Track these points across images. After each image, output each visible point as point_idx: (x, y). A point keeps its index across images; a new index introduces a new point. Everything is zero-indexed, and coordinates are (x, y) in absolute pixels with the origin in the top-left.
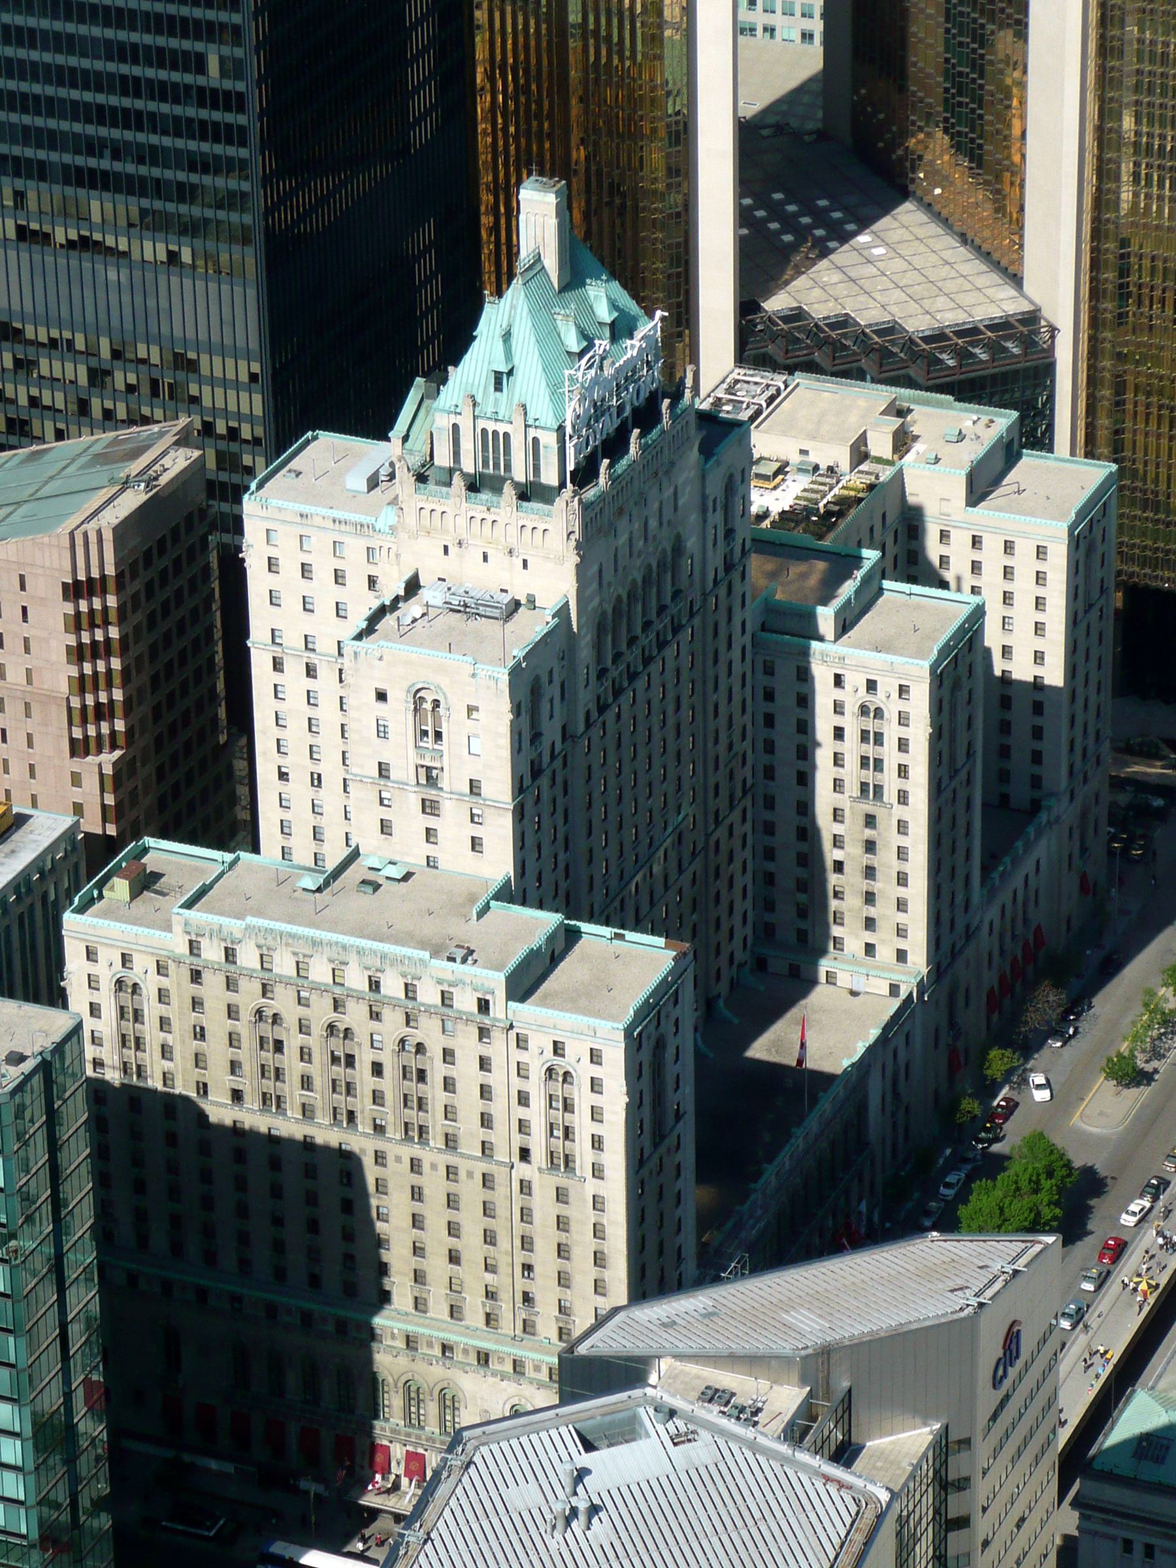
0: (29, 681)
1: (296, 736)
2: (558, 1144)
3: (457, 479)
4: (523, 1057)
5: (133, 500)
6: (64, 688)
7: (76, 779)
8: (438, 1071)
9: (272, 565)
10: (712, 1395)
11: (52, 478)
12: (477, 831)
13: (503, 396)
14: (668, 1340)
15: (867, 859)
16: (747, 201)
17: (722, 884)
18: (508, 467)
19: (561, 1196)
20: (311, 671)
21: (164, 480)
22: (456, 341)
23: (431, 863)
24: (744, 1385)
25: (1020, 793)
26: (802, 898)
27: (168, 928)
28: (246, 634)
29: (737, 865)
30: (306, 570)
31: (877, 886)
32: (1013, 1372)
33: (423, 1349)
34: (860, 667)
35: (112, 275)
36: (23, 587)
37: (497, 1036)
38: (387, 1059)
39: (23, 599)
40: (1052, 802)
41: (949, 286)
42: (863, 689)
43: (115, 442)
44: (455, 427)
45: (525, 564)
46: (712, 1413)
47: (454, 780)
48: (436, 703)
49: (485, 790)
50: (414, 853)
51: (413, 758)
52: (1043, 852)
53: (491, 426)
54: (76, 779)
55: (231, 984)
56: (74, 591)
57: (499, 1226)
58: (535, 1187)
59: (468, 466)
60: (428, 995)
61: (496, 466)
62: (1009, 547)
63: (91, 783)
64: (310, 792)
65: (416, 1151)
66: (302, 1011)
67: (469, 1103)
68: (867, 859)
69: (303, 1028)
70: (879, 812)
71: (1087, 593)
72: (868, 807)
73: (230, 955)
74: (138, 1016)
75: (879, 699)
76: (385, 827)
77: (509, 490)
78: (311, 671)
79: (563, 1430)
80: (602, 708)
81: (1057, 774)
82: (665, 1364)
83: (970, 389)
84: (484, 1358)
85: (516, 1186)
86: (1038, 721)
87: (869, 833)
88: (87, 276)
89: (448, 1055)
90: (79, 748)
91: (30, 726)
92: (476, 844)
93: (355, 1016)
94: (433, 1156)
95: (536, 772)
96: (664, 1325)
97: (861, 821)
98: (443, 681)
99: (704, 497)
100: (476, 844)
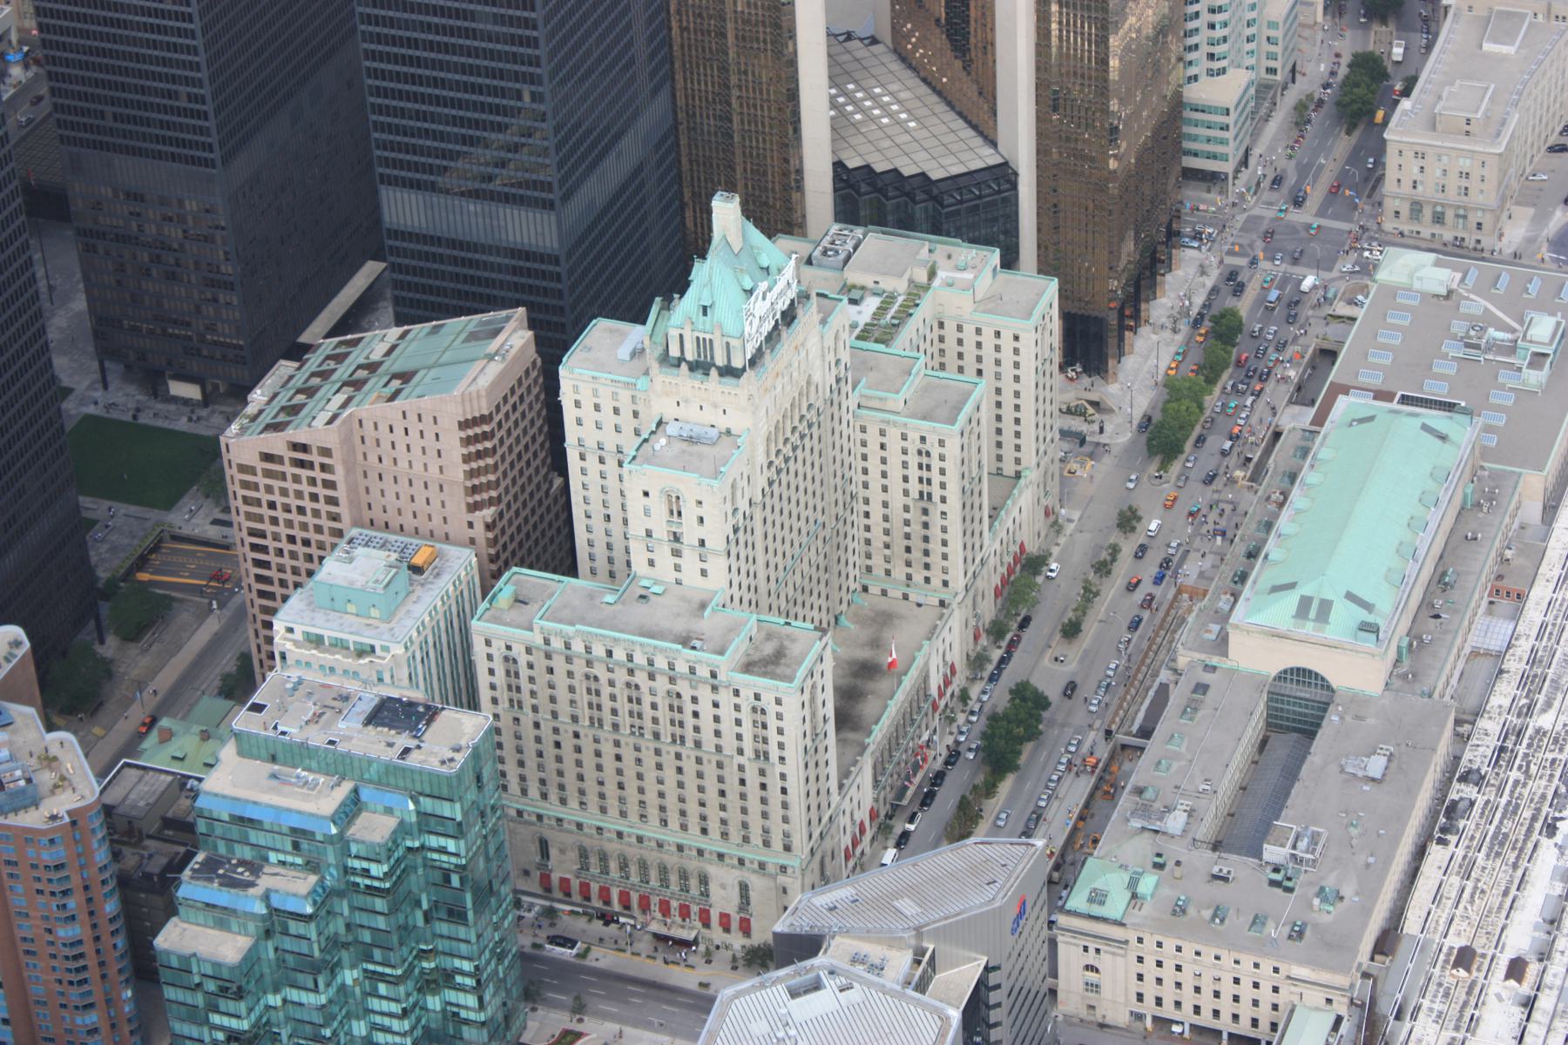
1: (594, 494)
2: (761, 746)
4: (737, 700)
5: (495, 368)
6: (461, 475)
7: (471, 525)
8: (689, 708)
10: (855, 960)
12: (704, 566)
15: (924, 532)
16: (833, 91)
17: (841, 552)
20: (602, 461)
21: (513, 352)
24: (874, 951)
25: (1009, 468)
26: (887, 552)
27: (531, 629)
28: (563, 439)
30: (597, 408)
31: (930, 546)
33: (687, 851)
34: (916, 429)
35: (472, 208)
39: (436, 429)
41: (954, 148)
42: (918, 441)
46: (859, 969)
51: (665, 528)
53: (701, 336)
54: (471, 525)
55: (569, 660)
56: (464, 425)
57: (723, 727)
62: (998, 334)
63: (479, 529)
64: (605, 525)
65: (678, 748)
66: (610, 675)
68: (924, 532)
69: (652, 693)
72: (924, 504)
73: (568, 646)
74: (517, 675)
76: (651, 563)
77: (714, 372)
78: (602, 461)
80: (771, 483)
81: (1029, 456)
84: (721, 856)
87: (924, 518)
88: (457, 210)
89: (694, 700)
90: (474, 507)
92: (704, 573)
93: (641, 678)
96: (831, 909)
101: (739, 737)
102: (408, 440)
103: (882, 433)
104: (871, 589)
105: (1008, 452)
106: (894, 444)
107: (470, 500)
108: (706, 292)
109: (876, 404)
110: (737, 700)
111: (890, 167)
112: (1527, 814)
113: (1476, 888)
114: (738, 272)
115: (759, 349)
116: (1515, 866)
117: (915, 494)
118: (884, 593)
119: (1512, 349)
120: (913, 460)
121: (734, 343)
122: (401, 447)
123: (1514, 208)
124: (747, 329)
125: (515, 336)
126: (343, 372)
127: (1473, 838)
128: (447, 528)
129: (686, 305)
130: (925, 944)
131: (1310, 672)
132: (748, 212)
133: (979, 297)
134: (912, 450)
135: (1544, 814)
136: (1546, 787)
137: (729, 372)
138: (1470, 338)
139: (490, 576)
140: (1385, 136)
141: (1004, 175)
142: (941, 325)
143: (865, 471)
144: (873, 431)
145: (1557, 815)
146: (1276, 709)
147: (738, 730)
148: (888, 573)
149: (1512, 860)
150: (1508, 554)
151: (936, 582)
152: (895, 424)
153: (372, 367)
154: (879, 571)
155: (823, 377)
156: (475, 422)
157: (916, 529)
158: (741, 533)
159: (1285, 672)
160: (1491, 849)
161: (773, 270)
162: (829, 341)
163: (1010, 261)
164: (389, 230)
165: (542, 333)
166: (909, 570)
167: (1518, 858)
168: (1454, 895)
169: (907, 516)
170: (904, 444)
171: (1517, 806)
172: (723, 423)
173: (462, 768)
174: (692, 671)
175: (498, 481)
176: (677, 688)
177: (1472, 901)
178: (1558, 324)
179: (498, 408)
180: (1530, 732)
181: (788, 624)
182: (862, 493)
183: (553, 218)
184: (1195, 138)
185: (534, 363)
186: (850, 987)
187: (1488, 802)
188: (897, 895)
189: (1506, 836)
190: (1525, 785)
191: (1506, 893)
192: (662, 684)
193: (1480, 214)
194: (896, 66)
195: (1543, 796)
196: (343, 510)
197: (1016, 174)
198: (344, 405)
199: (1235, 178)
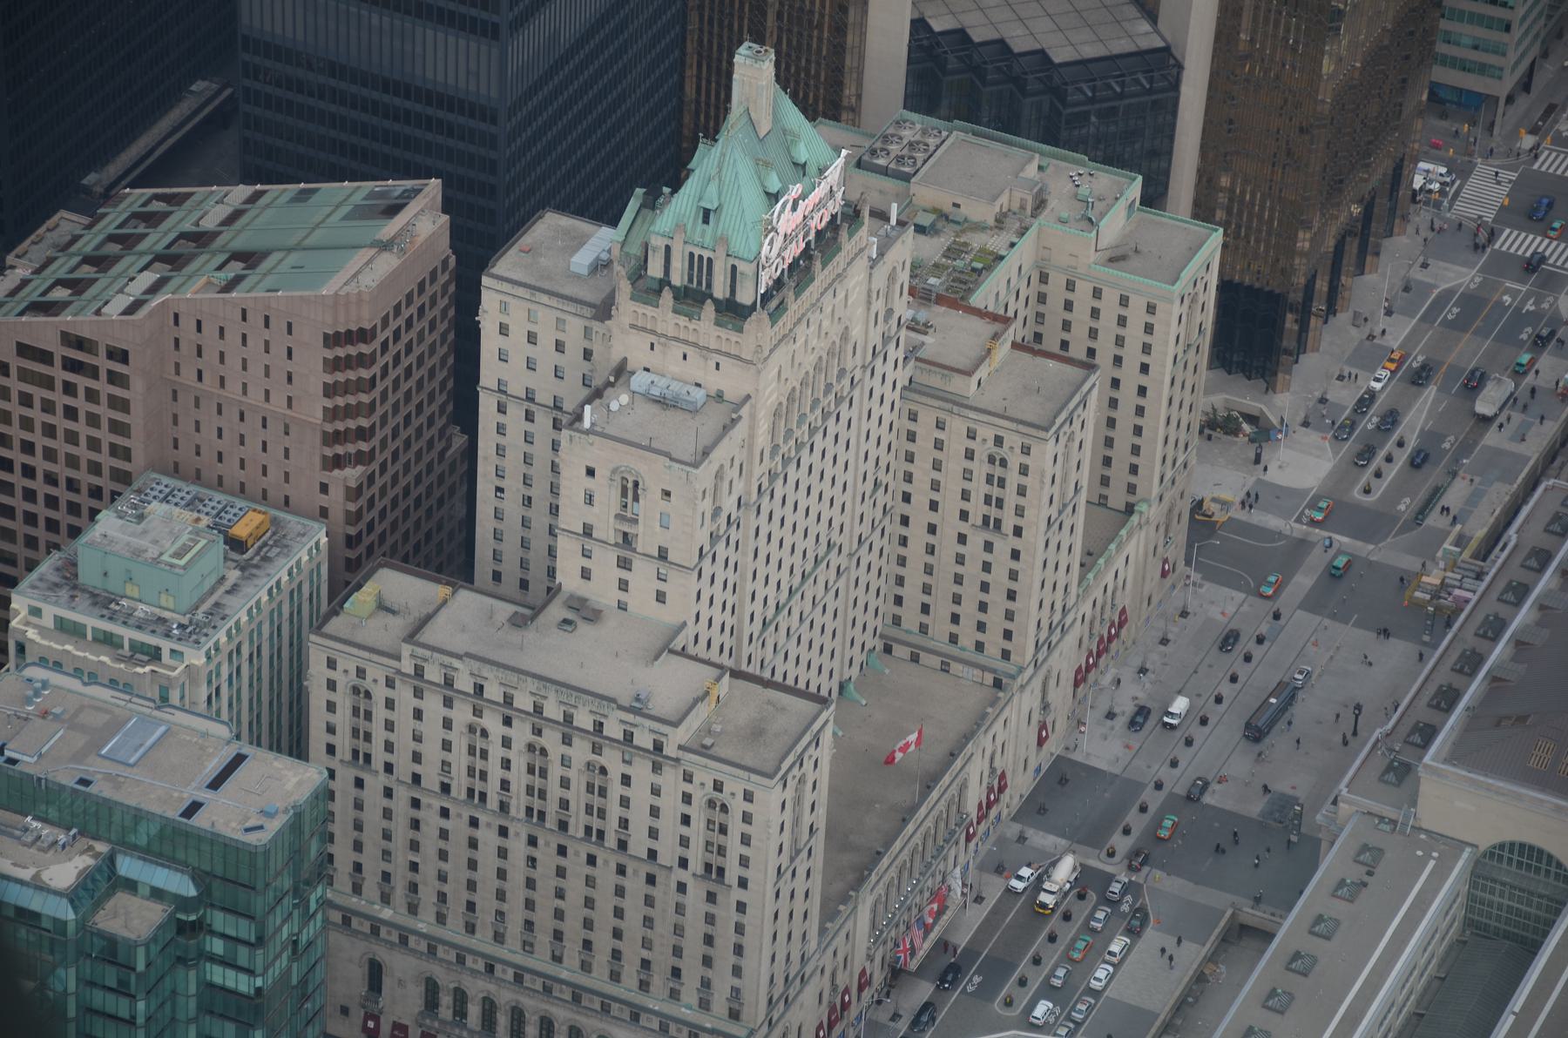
5: (387, 263)
7: (324, 488)
8: (616, 790)
9: (504, 330)
11: (317, 226)
12: (662, 586)
13: (709, 229)
18: (709, 285)
25: (1117, 499)
28: (476, 378)
36: (290, 332)
42: (991, 443)
43: (372, 195)
44: (668, 248)
48: (636, 484)
56: (332, 340)
59: (677, 279)
61: (699, 283)
65: (594, 850)
69: (565, 762)
74: (368, 716)
75: (1004, 452)
77: (709, 308)
80: (772, 476)
85: (674, 886)
92: (661, 597)
99: (870, 291)
100: (661, 597)
101: (684, 842)
111: (991, 35)
114: (762, 165)
117: (976, 518)
120: (980, 468)
125: (425, 219)
126: (157, 239)
129: (681, 205)
137: (733, 312)
139: (347, 571)
142: (1044, 278)
153: (201, 239)
156: (349, 337)
161: (812, 169)
163: (1154, 197)
173: (274, 840)
176: (602, 760)
185: (445, 262)
196: (136, 443)
197: (1180, 67)
198: (154, 289)
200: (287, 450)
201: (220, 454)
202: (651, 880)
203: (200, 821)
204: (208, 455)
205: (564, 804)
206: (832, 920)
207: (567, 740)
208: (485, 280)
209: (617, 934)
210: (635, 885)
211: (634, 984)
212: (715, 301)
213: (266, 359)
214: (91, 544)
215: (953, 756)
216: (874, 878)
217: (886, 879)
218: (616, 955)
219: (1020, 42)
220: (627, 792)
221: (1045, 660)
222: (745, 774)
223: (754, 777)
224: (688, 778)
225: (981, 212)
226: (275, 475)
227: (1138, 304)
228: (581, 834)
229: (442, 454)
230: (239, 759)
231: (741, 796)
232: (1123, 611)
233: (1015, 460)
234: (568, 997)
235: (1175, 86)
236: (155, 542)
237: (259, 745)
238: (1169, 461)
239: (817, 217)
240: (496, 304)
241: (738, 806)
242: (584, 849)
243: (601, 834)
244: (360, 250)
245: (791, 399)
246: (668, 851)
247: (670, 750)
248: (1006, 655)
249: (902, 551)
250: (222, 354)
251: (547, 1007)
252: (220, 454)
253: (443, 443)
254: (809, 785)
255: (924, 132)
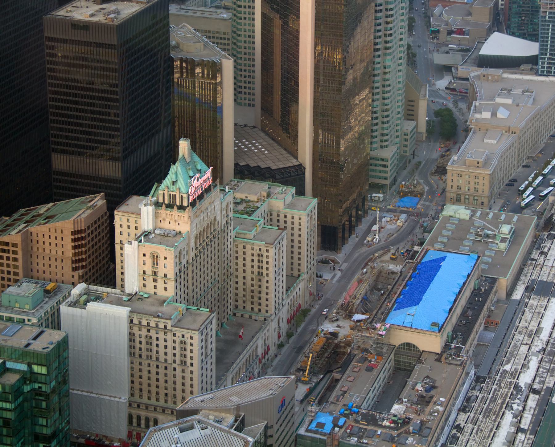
0: (63, 254)
3: (164, 205)
4: (175, 338)
5: (89, 212)
6: (71, 255)
7: (73, 276)
8: (155, 342)
9: (121, 226)
12: (166, 286)
14: (202, 405)
15: (259, 289)
17: (225, 296)
18: (175, 202)
19: (183, 371)
22: (165, 174)
23: (155, 293)
25: (296, 273)
26: (244, 299)
29: (229, 291)
30: (129, 227)
32: (283, 409)
34: (257, 245)
37: (169, 334)
38: (143, 340)
40: (303, 275)
42: (258, 250)
44: (164, 193)
45: (179, 224)
47: (161, 274)
48: (157, 256)
49: (168, 276)
50: (152, 291)
51: (151, 269)
52: (301, 286)
53: (172, 193)
54: (73, 276)
56: (73, 233)
58: (177, 369)
59: (166, 202)
60: (153, 324)
65: (149, 362)
67: (162, 350)
69: (140, 336)
70: (262, 278)
71: (311, 227)
72: (259, 277)
77: (175, 207)
79: (176, 428)
80: (196, 256)
81: (304, 268)
82: (203, 411)
83: (285, 182)
85: (172, 369)
86: (300, 256)
89: (157, 339)
90: (74, 269)
91: (63, 264)
92: (166, 289)
94: (153, 364)
95: (180, 271)
96: (202, 401)
97: (258, 280)
98: (159, 251)
100: (166, 289)
101: (175, 355)
102: (50, 240)
103: (244, 247)
104: (237, 315)
105: (296, 266)
106: (249, 252)
107: (74, 266)
108: (174, 176)
109: (242, 236)
110: (175, 338)
111: (256, 165)
112: (500, 401)
113: (478, 429)
115: (195, 200)
116: (495, 421)
117: (256, 273)
118: (242, 316)
119: (494, 237)
120: (256, 258)
121: (185, 196)
122: (47, 244)
123: (496, 199)
124: (190, 190)
125: (99, 201)
126: (27, 218)
127: (477, 410)
128: (63, 278)
130: (240, 413)
131: (412, 344)
132: (194, 147)
133: (287, 203)
134: (256, 254)
135: (507, 401)
136: (507, 392)
137: (182, 208)
138: (478, 232)
140: (447, 168)
141: (300, 168)
142: (271, 214)
143: (237, 264)
144: (241, 246)
145: (512, 402)
146: (398, 361)
147: (174, 351)
148: (244, 307)
149: (494, 418)
150: (492, 308)
151: (263, 311)
152: (249, 243)
153: (40, 215)
154: (241, 307)
155: (221, 220)
156: (79, 232)
157: (256, 288)
158: (182, 274)
159: (401, 345)
160: (485, 414)
161: (202, 171)
162: (224, 206)
163: (301, 192)
164: (54, 171)
165: (109, 198)
166: (252, 306)
167: (496, 418)
168: (469, 431)
169: (253, 282)
170: (253, 252)
171: (496, 399)
172: (178, 229)
173: (51, 350)
174: (157, 325)
175: (86, 251)
176: (150, 334)
177: (477, 433)
178: (512, 228)
179: (88, 227)
180: (501, 371)
181: (198, 309)
182: (235, 273)
183: (120, 164)
184: (375, 171)
185: (106, 213)
186: (206, 428)
187: (484, 397)
188: (230, 396)
189: (491, 409)
190: (499, 391)
191: (491, 431)
192: (144, 332)
193: (483, 198)
194: (262, 134)
195: (507, 395)
197: (304, 168)
198: (25, 227)
199: (391, 188)
200: (62, 267)
201: (44, 271)
202: (166, 368)
203: (30, 348)
204: (41, 272)
205: (140, 349)
206: (220, 380)
207: (140, 330)
208: (116, 213)
209: (158, 387)
210: (162, 370)
211: (163, 401)
212: (177, 206)
213: (56, 241)
214: (6, 294)
215: (253, 337)
216: (231, 370)
217: (235, 371)
218: (158, 393)
219: (263, 166)
220: (158, 342)
221: (278, 313)
222: (190, 331)
223: (193, 332)
224: (174, 335)
225: (253, 198)
226: (59, 275)
227: (296, 217)
228: (145, 358)
229: (107, 269)
230: (42, 332)
231: (189, 338)
232: (300, 304)
233: (265, 254)
234: (144, 408)
235: (304, 174)
236: (24, 291)
237: (48, 327)
238: (309, 262)
239: (205, 184)
240: (118, 215)
241: (189, 341)
242: (146, 362)
243: (151, 356)
244: (81, 211)
245: (200, 234)
246: (170, 358)
247: (169, 327)
248: (267, 311)
249: (237, 286)
250: (44, 242)
251: (138, 412)
252: (44, 271)
253: (107, 266)
254: (209, 336)
255: (238, 182)
